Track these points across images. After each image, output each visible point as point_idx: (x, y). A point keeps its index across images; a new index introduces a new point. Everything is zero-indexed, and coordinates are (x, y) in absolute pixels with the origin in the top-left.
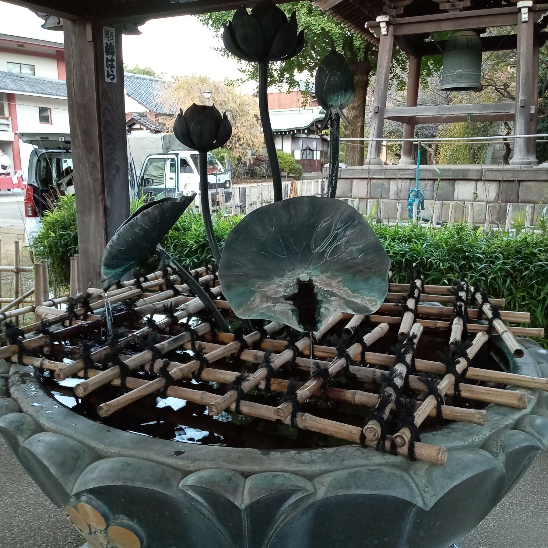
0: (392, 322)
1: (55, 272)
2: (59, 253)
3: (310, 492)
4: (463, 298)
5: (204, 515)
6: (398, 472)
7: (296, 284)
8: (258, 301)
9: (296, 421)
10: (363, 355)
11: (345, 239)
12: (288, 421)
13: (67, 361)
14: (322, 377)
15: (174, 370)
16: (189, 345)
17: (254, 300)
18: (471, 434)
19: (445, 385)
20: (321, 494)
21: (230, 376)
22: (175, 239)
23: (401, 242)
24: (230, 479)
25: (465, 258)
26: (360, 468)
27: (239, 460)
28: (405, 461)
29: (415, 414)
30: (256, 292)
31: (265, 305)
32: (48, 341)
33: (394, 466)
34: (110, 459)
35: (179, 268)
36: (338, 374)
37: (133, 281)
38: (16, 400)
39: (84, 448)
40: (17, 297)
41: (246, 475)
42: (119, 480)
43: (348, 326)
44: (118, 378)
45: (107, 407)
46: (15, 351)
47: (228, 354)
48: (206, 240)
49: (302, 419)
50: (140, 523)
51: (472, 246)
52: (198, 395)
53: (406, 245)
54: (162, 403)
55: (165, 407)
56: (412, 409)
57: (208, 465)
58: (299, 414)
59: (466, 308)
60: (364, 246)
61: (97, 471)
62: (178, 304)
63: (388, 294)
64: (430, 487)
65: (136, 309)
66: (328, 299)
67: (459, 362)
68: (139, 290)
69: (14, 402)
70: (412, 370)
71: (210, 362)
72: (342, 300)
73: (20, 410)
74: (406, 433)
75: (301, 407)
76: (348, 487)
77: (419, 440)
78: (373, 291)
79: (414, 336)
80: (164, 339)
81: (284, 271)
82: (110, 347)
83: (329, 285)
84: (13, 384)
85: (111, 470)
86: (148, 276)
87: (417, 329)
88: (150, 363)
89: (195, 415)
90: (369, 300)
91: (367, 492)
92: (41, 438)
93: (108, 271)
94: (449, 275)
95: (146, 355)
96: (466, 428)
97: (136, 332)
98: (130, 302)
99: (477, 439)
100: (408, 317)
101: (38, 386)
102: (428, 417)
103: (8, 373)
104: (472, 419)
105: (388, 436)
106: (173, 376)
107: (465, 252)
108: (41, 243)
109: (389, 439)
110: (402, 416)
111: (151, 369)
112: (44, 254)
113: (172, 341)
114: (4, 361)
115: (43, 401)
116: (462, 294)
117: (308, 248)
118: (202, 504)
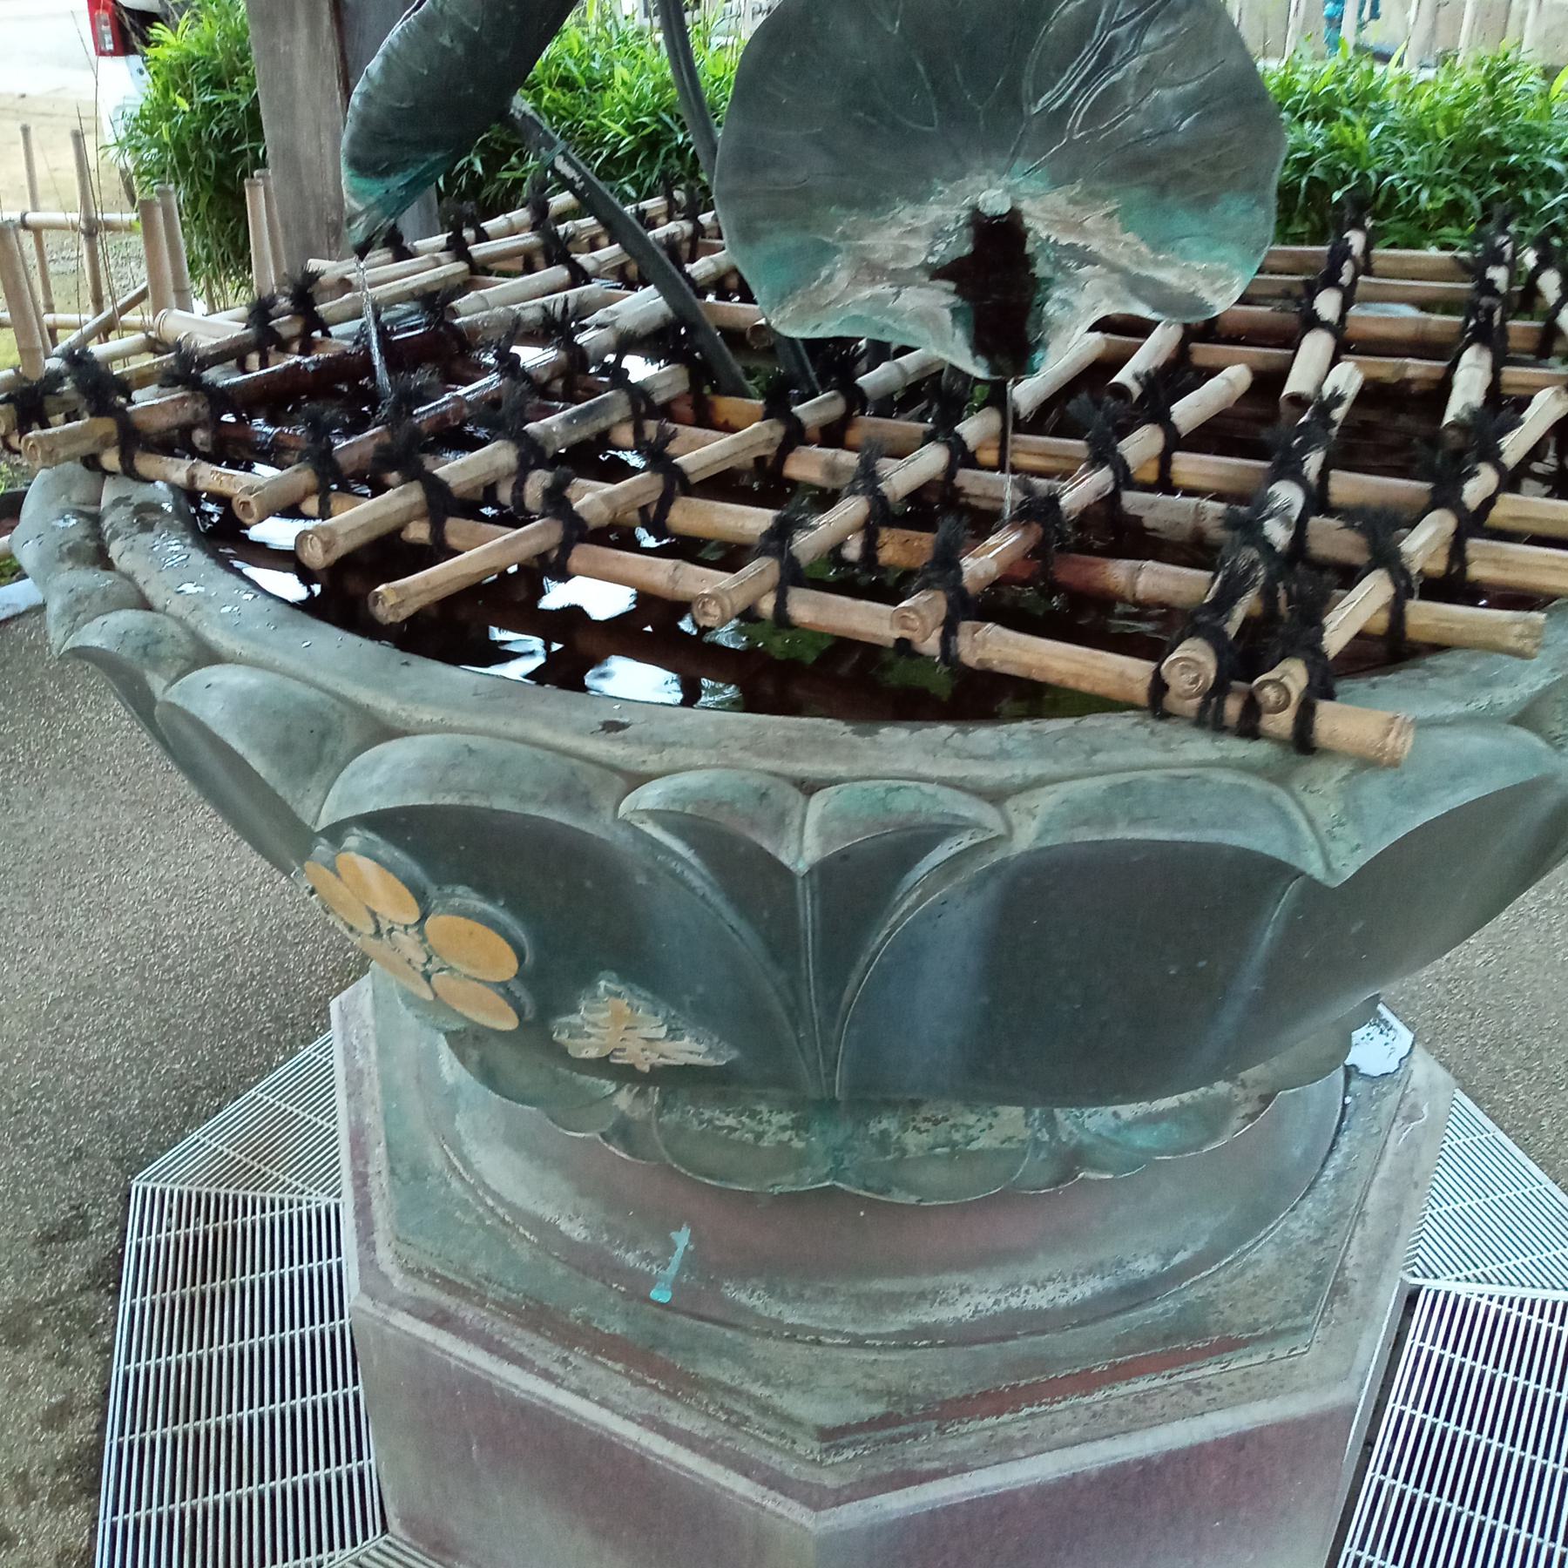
0: (1261, 366)
1: (203, 233)
2: (211, 163)
3: (993, 835)
4: (1497, 286)
5: (692, 890)
6: (1256, 784)
7: (967, 225)
8: (842, 278)
9: (956, 646)
10: (1165, 460)
11: (1137, 62)
12: (930, 645)
13: (265, 472)
14: (1037, 521)
15: (587, 498)
16: (625, 435)
17: (830, 278)
18: (1488, 684)
19: (1424, 543)
20: (1026, 838)
21: (755, 520)
22: (564, 119)
23: (1302, 119)
24: (764, 795)
25: (1505, 174)
26: (1144, 773)
27: (788, 748)
28: (1280, 757)
29: (1326, 620)
30: (836, 250)
31: (867, 292)
32: (204, 412)
33: (1246, 767)
34: (420, 739)
35: (584, 178)
36: (1086, 517)
37: (441, 239)
38: (129, 577)
39: (339, 706)
40: (99, 310)
41: (808, 787)
42: (449, 791)
43: (1123, 376)
44: (419, 518)
45: (399, 596)
46: (108, 435)
47: (747, 460)
48: (659, 120)
49: (974, 640)
50: (514, 907)
51: (1530, 133)
52: (664, 574)
53: (1317, 130)
54: (556, 596)
55: (563, 609)
56: (1312, 614)
57: (698, 757)
58: (965, 626)
59: (1503, 320)
60: (1204, 87)
61: (384, 768)
62: (583, 310)
63: (1271, 254)
64: (1349, 827)
65: (457, 321)
66: (1070, 275)
67: (1472, 474)
68: (461, 266)
69: (127, 583)
70: (1318, 501)
71: (694, 479)
72: (1116, 276)
73: (145, 605)
74: (1294, 674)
75: (971, 607)
76: (1109, 821)
77: (1330, 696)
78: (1222, 241)
79: (1337, 399)
80: (551, 412)
81: (929, 180)
82: (388, 429)
83: (1077, 227)
84: (115, 535)
85: (424, 765)
86: (488, 225)
87: (1348, 378)
88: (513, 480)
89: (649, 629)
90: (1205, 274)
91: (1162, 835)
92: (214, 680)
93: (363, 184)
94: (1446, 230)
95: (498, 455)
96: (1475, 667)
97: (462, 391)
98: (435, 301)
99: (1507, 696)
100: (1315, 346)
101: (188, 541)
102: (1361, 635)
103: (99, 503)
104: (1498, 638)
105: (1235, 684)
106: (585, 515)
107: (1507, 152)
108: (152, 134)
109: (1240, 692)
110: (1286, 627)
111: (518, 497)
112: (164, 172)
113: (574, 416)
114: (80, 468)
115: (209, 579)
116: (1498, 275)
117: (1013, 99)
118: (680, 859)
